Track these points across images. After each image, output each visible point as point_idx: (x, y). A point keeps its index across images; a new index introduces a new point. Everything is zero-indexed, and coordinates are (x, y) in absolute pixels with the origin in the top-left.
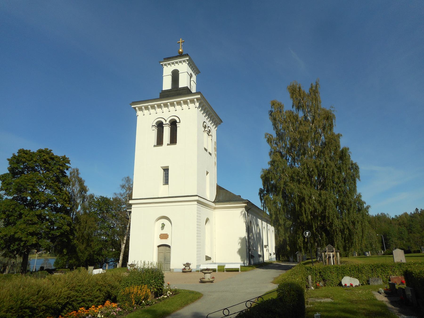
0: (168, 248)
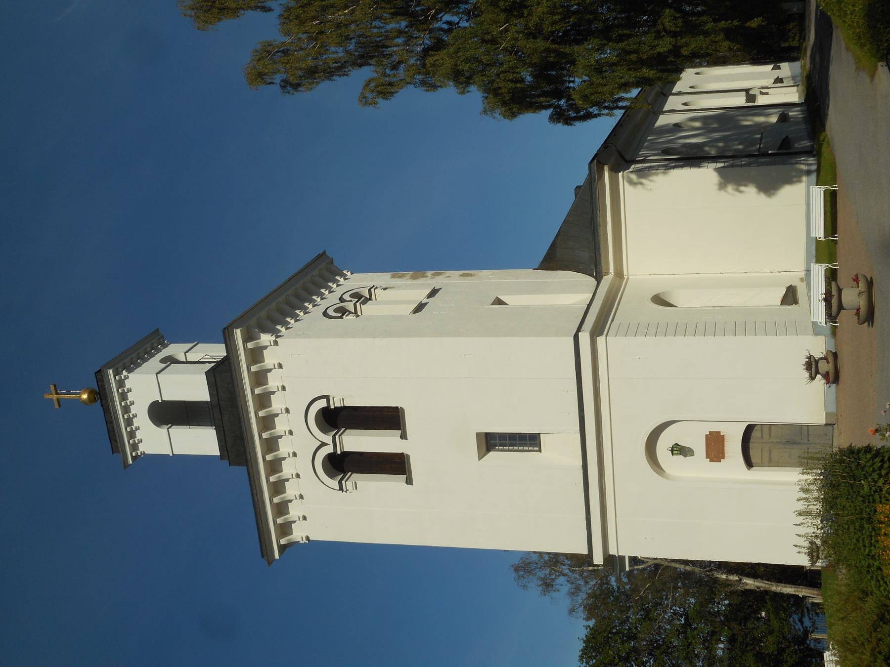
0: (755, 434)
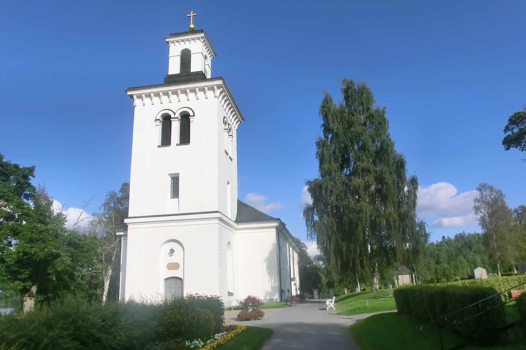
0: (179, 282)
